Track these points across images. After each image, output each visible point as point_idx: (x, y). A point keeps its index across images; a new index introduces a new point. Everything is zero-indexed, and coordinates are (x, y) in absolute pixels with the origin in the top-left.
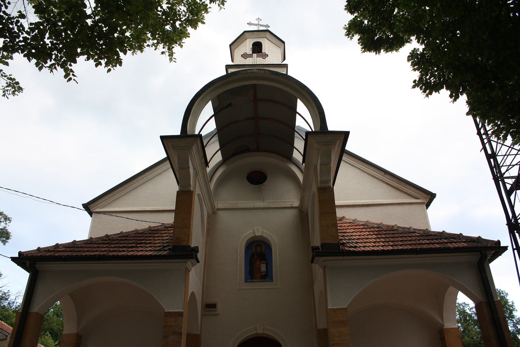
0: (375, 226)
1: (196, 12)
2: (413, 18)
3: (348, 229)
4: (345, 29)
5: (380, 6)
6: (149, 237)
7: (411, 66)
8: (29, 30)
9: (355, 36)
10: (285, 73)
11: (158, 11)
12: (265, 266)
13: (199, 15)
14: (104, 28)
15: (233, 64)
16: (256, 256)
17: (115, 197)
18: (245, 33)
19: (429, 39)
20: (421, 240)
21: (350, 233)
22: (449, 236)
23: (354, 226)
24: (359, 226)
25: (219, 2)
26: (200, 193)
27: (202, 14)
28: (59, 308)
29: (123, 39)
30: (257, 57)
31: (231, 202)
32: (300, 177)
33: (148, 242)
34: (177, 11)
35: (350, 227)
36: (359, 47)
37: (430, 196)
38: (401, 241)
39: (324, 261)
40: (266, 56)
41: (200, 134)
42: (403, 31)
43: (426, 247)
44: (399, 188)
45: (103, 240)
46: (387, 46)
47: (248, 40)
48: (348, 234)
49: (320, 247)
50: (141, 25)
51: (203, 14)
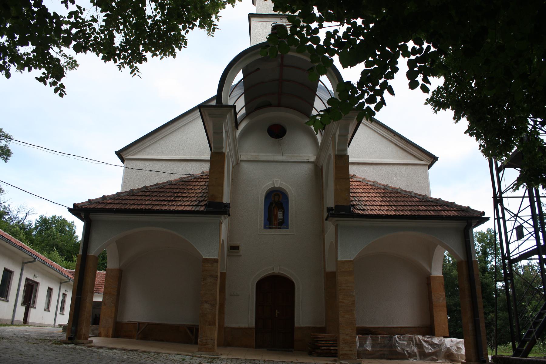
0: (382, 187)
8: (99, 31)
12: (282, 214)
16: (274, 205)
20: (419, 205)
22: (443, 203)
28: (61, 224)
31: (253, 154)
37: (433, 159)
38: (402, 206)
39: (336, 221)
43: (422, 214)
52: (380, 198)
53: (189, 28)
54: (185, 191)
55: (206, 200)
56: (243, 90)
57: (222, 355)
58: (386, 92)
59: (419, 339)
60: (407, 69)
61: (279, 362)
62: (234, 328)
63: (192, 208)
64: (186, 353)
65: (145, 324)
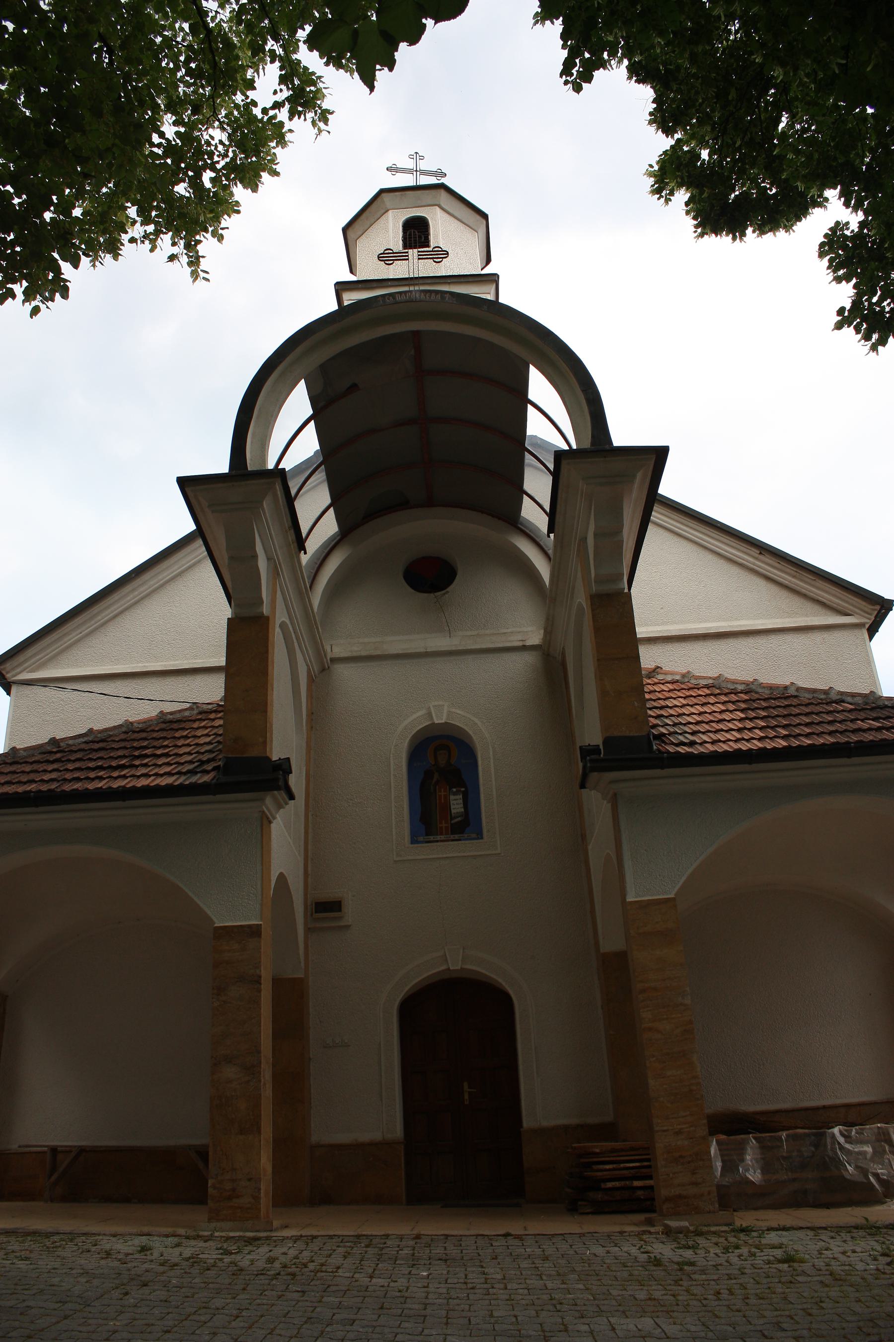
0: (740, 687)
1: (254, 145)
2: (833, 140)
3: (672, 698)
4: (651, 177)
5: (743, 110)
6: (161, 741)
7: (829, 271)
9: (677, 194)
10: (490, 297)
11: (153, 145)
12: (461, 801)
13: (263, 152)
14: (13, 199)
15: (353, 278)
16: (436, 776)
17: (66, 639)
18: (384, 195)
19: (875, 197)
20: (858, 720)
21: (677, 709)
23: (685, 689)
24: (698, 689)
25: (313, 115)
26: (288, 622)
27: (270, 149)
29: (67, 225)
30: (419, 259)
31: (366, 640)
32: (544, 569)
33: (159, 752)
34: (203, 142)
35: (676, 692)
36: (689, 223)
37: (878, 607)
38: (807, 725)
40: (441, 255)
41: (280, 467)
42: (804, 176)
43: (871, 738)
44: (798, 588)
45: (44, 753)
46: (763, 217)
47: (390, 212)
48: (672, 712)
49: (601, 747)
50: (109, 185)
51: (274, 148)
57: (286, 1227)
61: (464, 1238)
62: (340, 1147)
64: (170, 1230)
65: (71, 1151)
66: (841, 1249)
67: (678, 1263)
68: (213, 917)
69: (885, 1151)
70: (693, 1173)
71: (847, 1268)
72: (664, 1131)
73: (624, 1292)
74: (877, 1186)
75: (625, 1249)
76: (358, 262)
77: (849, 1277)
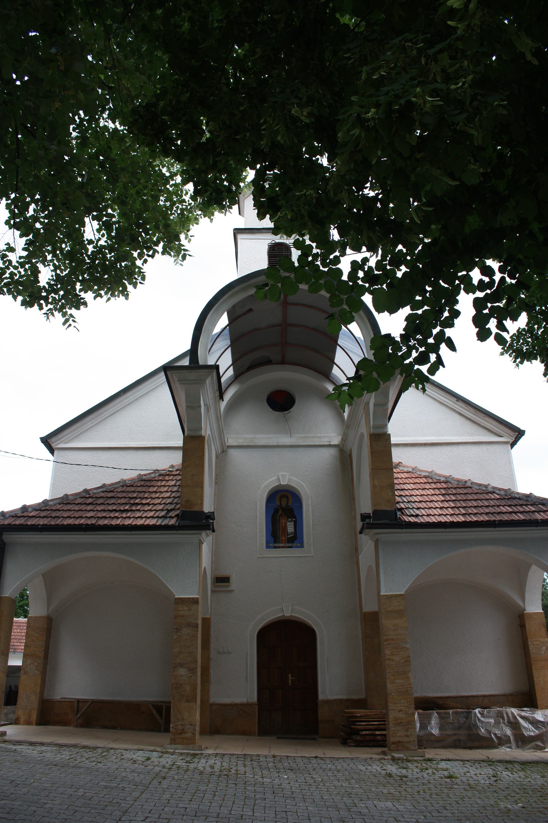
0: (443, 479)
8: (17, 265)
16: (280, 512)
17: (84, 427)
31: (246, 436)
37: (517, 434)
39: (376, 534)
43: (506, 518)
44: (476, 421)
52: (440, 496)
53: (149, 256)
54: (146, 496)
55: (178, 509)
56: (229, 341)
58: (443, 346)
59: (512, 714)
60: (474, 312)
62: (225, 705)
63: (158, 521)
65: (88, 702)
66: (474, 773)
67: (400, 776)
68: (174, 593)
69: (500, 722)
70: (406, 731)
71: (476, 782)
72: (393, 710)
73: (377, 790)
74: (495, 739)
75: (374, 767)
76: (245, 213)
77: (477, 787)
